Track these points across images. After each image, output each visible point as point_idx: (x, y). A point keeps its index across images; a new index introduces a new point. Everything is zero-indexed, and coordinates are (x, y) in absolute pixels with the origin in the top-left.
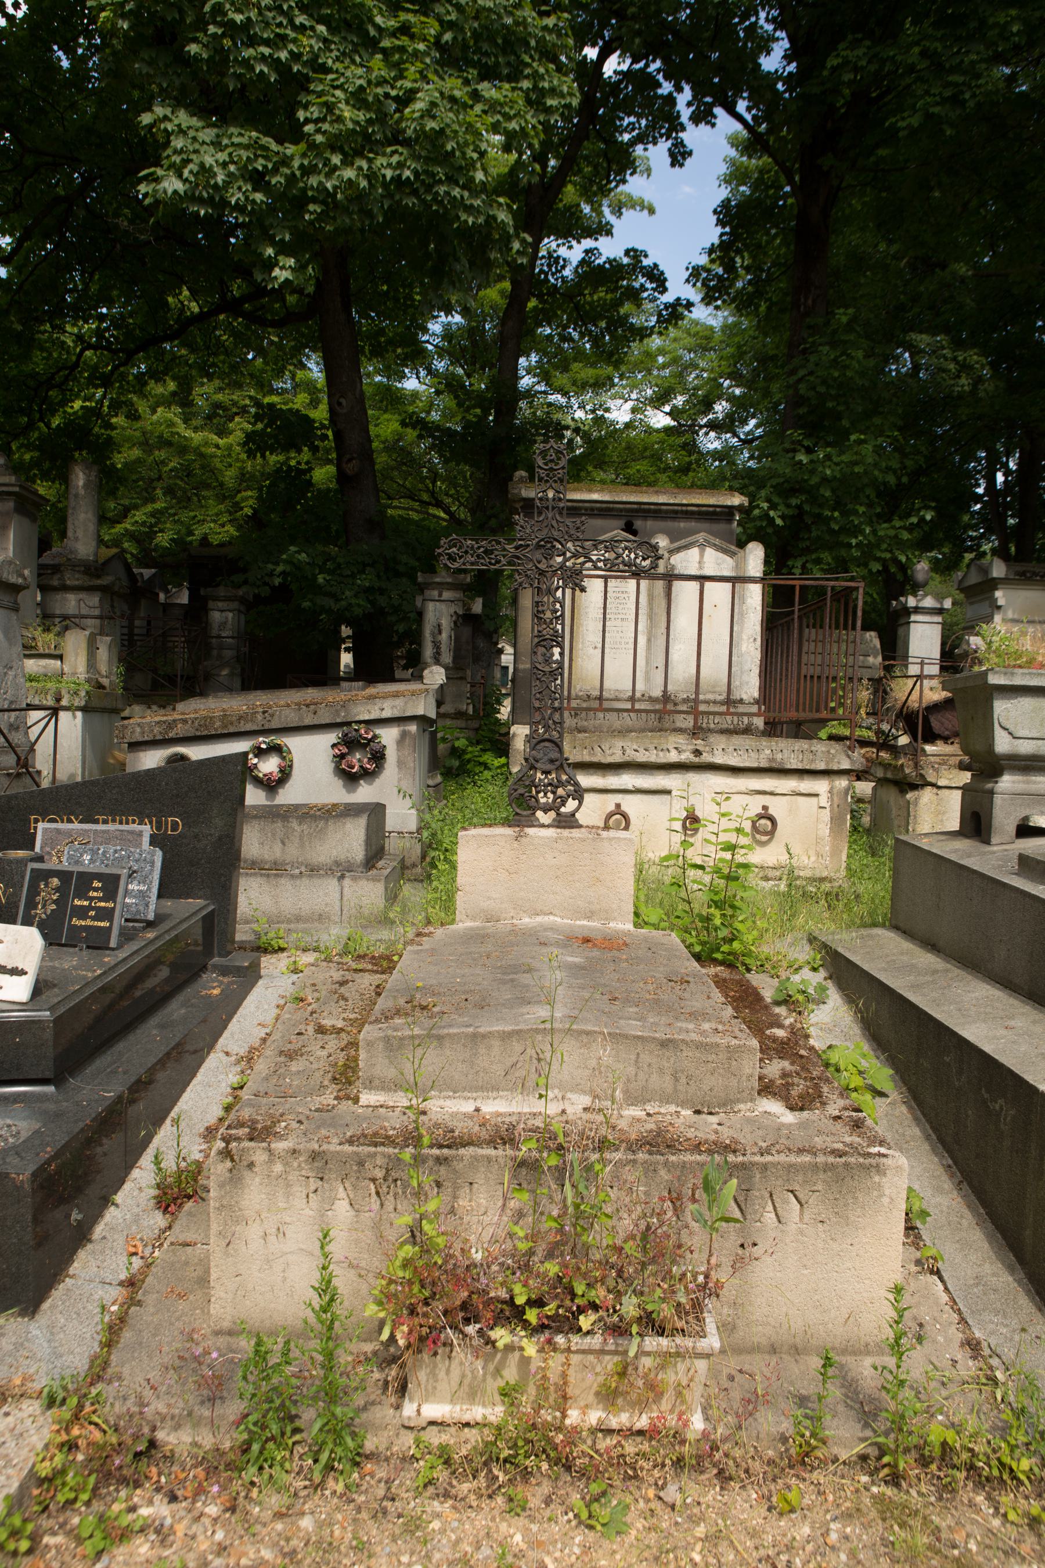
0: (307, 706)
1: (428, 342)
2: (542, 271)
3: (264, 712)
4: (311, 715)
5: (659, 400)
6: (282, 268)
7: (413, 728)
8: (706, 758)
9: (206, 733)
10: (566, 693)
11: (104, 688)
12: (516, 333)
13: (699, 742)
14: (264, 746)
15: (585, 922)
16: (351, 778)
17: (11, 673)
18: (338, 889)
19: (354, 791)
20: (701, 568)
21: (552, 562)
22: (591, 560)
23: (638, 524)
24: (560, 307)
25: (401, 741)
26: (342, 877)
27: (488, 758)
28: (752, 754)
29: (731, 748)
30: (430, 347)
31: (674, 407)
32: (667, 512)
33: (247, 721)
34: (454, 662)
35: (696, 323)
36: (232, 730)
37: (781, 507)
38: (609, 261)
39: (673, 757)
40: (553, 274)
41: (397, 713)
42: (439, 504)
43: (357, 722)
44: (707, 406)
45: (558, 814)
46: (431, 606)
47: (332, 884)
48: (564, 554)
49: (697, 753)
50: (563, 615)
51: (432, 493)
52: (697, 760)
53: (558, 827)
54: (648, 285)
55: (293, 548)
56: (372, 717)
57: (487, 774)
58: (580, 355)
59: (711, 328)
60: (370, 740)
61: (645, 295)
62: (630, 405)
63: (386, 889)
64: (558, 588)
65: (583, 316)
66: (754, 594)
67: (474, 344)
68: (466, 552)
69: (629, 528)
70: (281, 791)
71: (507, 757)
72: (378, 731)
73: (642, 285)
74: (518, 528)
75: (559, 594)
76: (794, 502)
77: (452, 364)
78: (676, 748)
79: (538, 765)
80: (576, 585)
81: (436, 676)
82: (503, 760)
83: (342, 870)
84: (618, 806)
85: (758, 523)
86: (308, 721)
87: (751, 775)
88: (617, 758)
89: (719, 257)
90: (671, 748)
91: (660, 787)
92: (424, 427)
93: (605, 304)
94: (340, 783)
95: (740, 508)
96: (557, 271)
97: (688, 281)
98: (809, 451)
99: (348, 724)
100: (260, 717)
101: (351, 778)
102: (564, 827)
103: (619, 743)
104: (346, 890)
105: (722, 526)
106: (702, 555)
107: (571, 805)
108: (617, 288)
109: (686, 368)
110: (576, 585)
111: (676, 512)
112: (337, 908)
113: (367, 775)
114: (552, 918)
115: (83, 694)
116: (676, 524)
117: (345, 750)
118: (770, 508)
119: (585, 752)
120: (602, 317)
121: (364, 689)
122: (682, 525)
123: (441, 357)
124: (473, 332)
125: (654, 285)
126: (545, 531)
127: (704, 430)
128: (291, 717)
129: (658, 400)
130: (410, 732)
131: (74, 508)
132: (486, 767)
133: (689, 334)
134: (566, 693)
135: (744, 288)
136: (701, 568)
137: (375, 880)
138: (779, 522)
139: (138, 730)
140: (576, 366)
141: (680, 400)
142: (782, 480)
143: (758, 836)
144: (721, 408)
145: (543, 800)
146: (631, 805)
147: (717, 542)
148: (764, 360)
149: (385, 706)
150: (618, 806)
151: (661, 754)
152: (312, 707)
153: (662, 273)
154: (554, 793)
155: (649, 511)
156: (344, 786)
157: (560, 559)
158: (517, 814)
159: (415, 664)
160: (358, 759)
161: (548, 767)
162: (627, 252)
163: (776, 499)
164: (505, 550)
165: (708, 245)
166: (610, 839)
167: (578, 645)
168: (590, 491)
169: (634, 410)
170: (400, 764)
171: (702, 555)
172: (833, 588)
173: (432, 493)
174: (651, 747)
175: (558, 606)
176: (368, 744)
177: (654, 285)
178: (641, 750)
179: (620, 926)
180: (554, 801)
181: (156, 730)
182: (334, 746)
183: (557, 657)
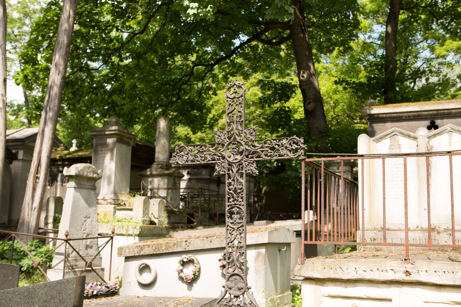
3: (186, 241)
4: (209, 242)
6: (192, 8)
8: (414, 277)
9: (158, 252)
11: (154, 224)
14: (185, 260)
17: (89, 220)
20: (450, 146)
23: (438, 122)
28: (449, 275)
29: (432, 271)
32: (455, 113)
33: (177, 246)
36: (170, 251)
39: (390, 276)
49: (408, 273)
52: (407, 278)
70: (194, 285)
86: (207, 247)
87: (450, 289)
90: (388, 270)
100: (184, 244)
106: (450, 138)
115: (138, 228)
119: (332, 271)
121: (267, 224)
128: (199, 245)
130: (261, 253)
131: (158, 138)
139: (128, 250)
151: (382, 273)
155: (444, 114)
161: (238, 293)
170: (257, 271)
171: (450, 138)
172: (324, 161)
178: (368, 270)
181: (136, 250)
182: (220, 260)
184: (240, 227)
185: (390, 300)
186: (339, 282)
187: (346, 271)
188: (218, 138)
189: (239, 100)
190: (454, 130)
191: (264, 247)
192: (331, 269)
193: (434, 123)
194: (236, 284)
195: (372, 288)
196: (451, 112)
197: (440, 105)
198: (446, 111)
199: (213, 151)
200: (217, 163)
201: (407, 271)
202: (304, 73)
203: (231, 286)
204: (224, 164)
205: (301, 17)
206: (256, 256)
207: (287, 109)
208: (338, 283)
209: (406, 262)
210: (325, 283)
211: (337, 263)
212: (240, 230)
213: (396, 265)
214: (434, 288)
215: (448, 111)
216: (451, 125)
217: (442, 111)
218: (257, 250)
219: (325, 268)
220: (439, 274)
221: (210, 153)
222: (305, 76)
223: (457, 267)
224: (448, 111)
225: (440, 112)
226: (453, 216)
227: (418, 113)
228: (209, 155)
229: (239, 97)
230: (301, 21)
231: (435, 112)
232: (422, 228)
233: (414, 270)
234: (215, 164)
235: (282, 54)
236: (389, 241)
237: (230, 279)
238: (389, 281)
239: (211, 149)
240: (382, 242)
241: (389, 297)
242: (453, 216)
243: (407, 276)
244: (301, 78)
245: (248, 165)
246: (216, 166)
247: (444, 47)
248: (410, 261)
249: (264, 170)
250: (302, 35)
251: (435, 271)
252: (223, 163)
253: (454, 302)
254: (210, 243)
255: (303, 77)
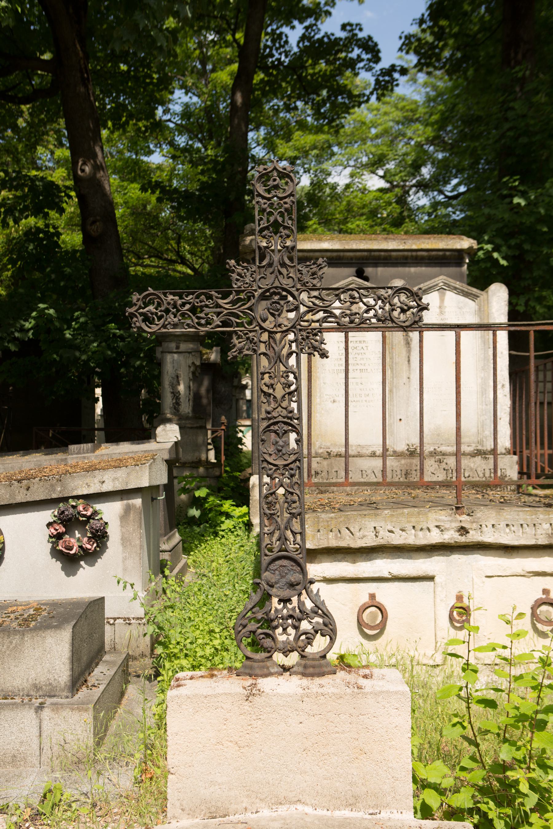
0: (19, 481)
1: (169, 120)
2: (266, 46)
5: (377, 162)
7: (138, 502)
8: (474, 537)
10: (305, 451)
12: (246, 112)
13: (464, 517)
15: (346, 813)
16: (70, 561)
18: (35, 722)
19: (74, 574)
21: (280, 320)
22: (333, 315)
23: (369, 271)
24: (284, 79)
25: (124, 517)
26: (41, 707)
27: (227, 506)
28: (527, 529)
30: (172, 125)
31: (387, 172)
34: (194, 410)
35: (403, 99)
37: (504, 249)
38: (326, 35)
39: (435, 537)
40: (277, 49)
41: (119, 486)
42: (184, 261)
43: (74, 497)
44: (416, 167)
45: (303, 657)
46: (169, 358)
47: (27, 718)
48: (297, 308)
49: (463, 531)
50: (298, 389)
51: (178, 253)
52: (462, 539)
53: (304, 675)
54: (365, 56)
55: (41, 306)
56: (92, 491)
57: (228, 524)
58: (302, 125)
59: (416, 102)
60: (89, 518)
61: (361, 65)
62: (348, 170)
63: (95, 718)
64: (290, 354)
65: (307, 88)
66: (503, 337)
67: (210, 120)
68: (167, 311)
69: (360, 274)
71: (248, 506)
72: (98, 507)
73: (359, 56)
74: (235, 276)
75: (292, 361)
76: (513, 242)
77: (191, 139)
78: (439, 526)
79: (274, 591)
80: (315, 348)
81: (169, 434)
82: (244, 509)
83: (39, 697)
84: (372, 596)
85: (483, 265)
86: (21, 498)
87: (526, 552)
88: (370, 541)
89: (429, 27)
91: (421, 573)
92: (167, 193)
93: (325, 74)
94: (59, 565)
95: (470, 252)
96: (281, 46)
97: (401, 49)
98: (523, 195)
99: (65, 499)
101: (70, 561)
102: (312, 675)
103: (370, 524)
104: (45, 724)
105: (452, 270)
106: (442, 300)
107: (320, 643)
108: (336, 59)
109: (396, 138)
110: (315, 348)
111: (406, 258)
112: (36, 747)
113: (89, 557)
114: (300, 807)
116: (407, 269)
117: (62, 529)
118: (494, 250)
119: (331, 535)
120: (323, 87)
121: (93, 451)
122: (413, 270)
123: (180, 133)
124: (209, 111)
125: (369, 56)
126: (270, 279)
127: (414, 189)
129: (373, 165)
130: (134, 506)
132: (228, 516)
133: (397, 108)
134: (305, 451)
135: (452, 55)
136: (441, 313)
137: (80, 707)
138: (503, 262)
140: (297, 134)
141: (391, 166)
142: (500, 225)
143: (539, 626)
144: (426, 171)
145: (282, 638)
146: (385, 593)
147: (458, 284)
148: (470, 121)
149: (105, 478)
150: (372, 596)
151: (420, 534)
152: (25, 482)
153: (376, 45)
154: (296, 628)
156: (63, 569)
157: (292, 315)
158: (248, 658)
159: (157, 417)
160: (76, 540)
161: (286, 593)
162: (343, 27)
163: (498, 241)
164: (218, 306)
165: (419, 16)
166: (376, 694)
167: (316, 400)
168: (320, 240)
169: (352, 176)
170: (125, 541)
171: (442, 300)
173: (178, 253)
174: (409, 526)
175: (291, 376)
176: (87, 522)
177: (369, 56)
179: (396, 816)
180: (297, 638)
182: (49, 525)
183: (293, 445)
184: (291, 463)
185: (431, 578)
186: (342, 553)
187: (358, 534)
188: (237, 280)
189: (285, 203)
190: (449, 286)
191: (140, 495)
192: (331, 531)
193: (363, 272)
194: (282, 577)
195: (401, 560)
196: (390, 256)
197: (375, 242)
198: (383, 253)
199: (227, 306)
200: (235, 332)
201: (462, 528)
202: (84, 163)
203: (273, 581)
204: (253, 334)
205: (81, 54)
206: (122, 512)
207: (51, 230)
208: (340, 556)
209: (459, 511)
210: (315, 557)
211: (341, 519)
212: (292, 469)
213: (443, 518)
214: (501, 552)
215: (386, 254)
216: (445, 277)
217: (377, 254)
218: (125, 502)
219: (319, 531)
220: (513, 528)
221: (218, 310)
222: (87, 169)
223: (541, 516)
224: (386, 254)
225: (373, 253)
226: (458, 429)
227: (339, 254)
228: (218, 314)
229: (285, 198)
230: (82, 62)
231: (366, 254)
232: (395, 452)
233: (474, 524)
234: (230, 334)
235: (21, 122)
236: (355, 477)
237: (272, 567)
238: (429, 546)
239: (221, 302)
240: (381, 480)
241: (431, 574)
242: (458, 429)
243: (461, 535)
244: (79, 172)
245: (308, 337)
246: (235, 337)
247: (291, 144)
248: (465, 510)
249: (10, 345)
250: (82, 89)
251: (507, 525)
252: (251, 331)
253: (532, 572)
254: (25, 492)
255: (83, 171)
